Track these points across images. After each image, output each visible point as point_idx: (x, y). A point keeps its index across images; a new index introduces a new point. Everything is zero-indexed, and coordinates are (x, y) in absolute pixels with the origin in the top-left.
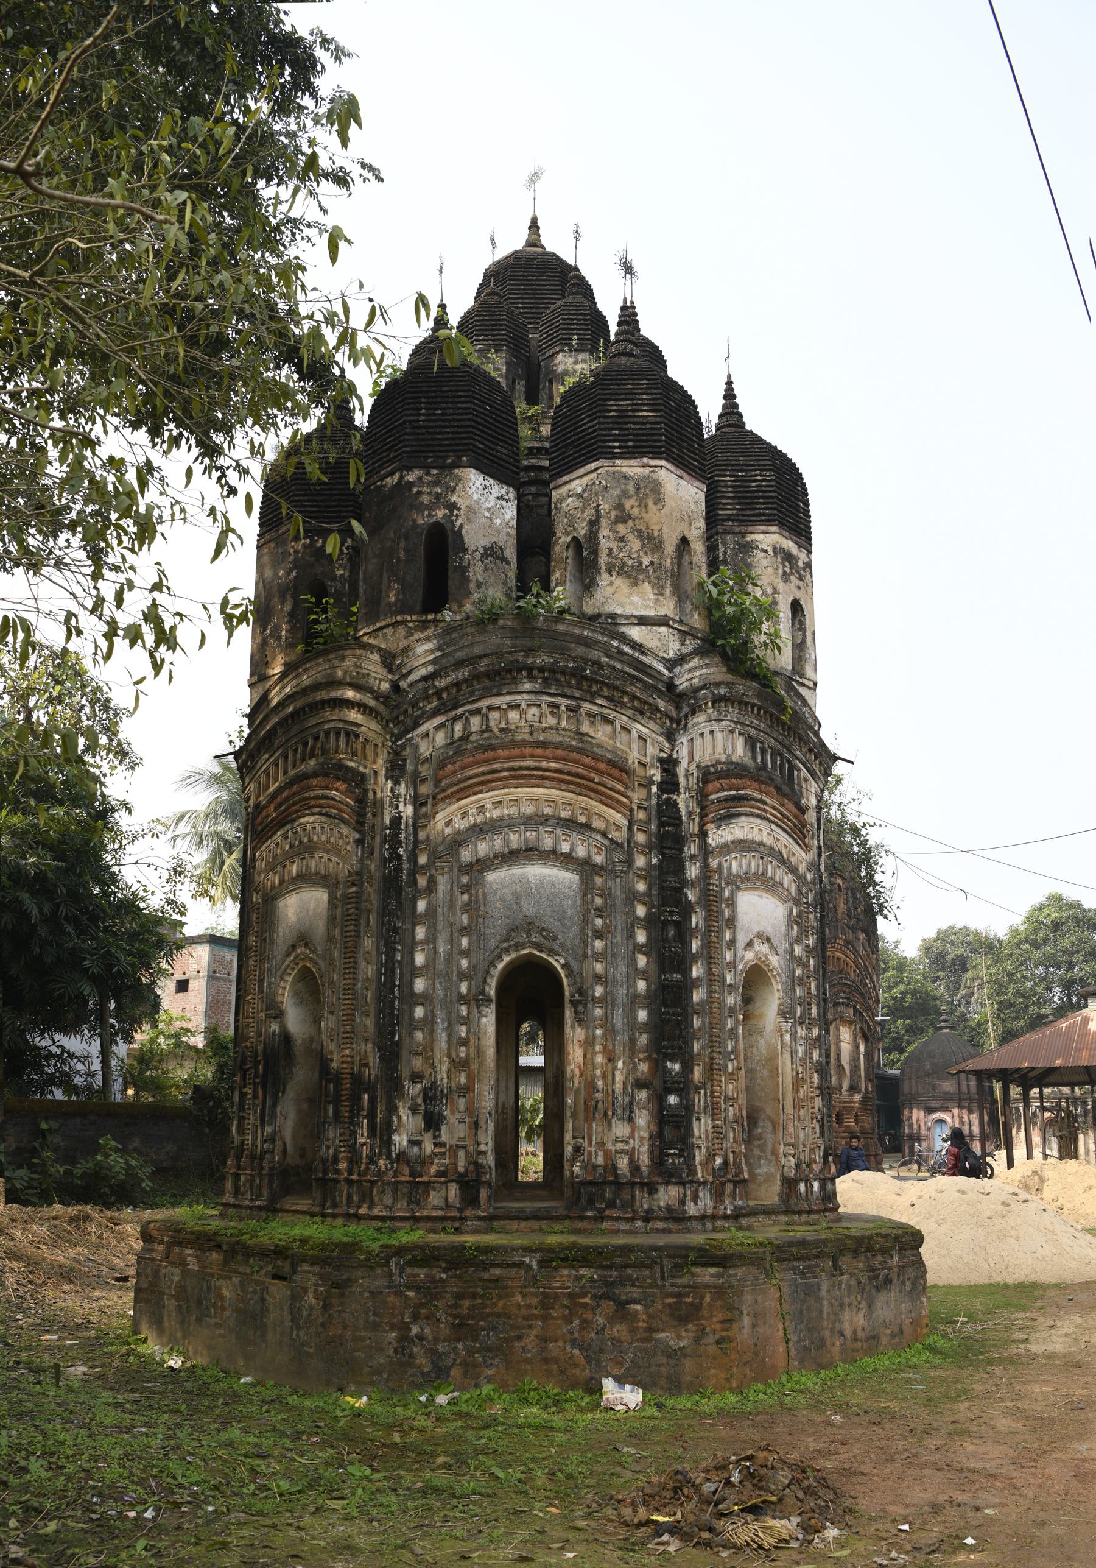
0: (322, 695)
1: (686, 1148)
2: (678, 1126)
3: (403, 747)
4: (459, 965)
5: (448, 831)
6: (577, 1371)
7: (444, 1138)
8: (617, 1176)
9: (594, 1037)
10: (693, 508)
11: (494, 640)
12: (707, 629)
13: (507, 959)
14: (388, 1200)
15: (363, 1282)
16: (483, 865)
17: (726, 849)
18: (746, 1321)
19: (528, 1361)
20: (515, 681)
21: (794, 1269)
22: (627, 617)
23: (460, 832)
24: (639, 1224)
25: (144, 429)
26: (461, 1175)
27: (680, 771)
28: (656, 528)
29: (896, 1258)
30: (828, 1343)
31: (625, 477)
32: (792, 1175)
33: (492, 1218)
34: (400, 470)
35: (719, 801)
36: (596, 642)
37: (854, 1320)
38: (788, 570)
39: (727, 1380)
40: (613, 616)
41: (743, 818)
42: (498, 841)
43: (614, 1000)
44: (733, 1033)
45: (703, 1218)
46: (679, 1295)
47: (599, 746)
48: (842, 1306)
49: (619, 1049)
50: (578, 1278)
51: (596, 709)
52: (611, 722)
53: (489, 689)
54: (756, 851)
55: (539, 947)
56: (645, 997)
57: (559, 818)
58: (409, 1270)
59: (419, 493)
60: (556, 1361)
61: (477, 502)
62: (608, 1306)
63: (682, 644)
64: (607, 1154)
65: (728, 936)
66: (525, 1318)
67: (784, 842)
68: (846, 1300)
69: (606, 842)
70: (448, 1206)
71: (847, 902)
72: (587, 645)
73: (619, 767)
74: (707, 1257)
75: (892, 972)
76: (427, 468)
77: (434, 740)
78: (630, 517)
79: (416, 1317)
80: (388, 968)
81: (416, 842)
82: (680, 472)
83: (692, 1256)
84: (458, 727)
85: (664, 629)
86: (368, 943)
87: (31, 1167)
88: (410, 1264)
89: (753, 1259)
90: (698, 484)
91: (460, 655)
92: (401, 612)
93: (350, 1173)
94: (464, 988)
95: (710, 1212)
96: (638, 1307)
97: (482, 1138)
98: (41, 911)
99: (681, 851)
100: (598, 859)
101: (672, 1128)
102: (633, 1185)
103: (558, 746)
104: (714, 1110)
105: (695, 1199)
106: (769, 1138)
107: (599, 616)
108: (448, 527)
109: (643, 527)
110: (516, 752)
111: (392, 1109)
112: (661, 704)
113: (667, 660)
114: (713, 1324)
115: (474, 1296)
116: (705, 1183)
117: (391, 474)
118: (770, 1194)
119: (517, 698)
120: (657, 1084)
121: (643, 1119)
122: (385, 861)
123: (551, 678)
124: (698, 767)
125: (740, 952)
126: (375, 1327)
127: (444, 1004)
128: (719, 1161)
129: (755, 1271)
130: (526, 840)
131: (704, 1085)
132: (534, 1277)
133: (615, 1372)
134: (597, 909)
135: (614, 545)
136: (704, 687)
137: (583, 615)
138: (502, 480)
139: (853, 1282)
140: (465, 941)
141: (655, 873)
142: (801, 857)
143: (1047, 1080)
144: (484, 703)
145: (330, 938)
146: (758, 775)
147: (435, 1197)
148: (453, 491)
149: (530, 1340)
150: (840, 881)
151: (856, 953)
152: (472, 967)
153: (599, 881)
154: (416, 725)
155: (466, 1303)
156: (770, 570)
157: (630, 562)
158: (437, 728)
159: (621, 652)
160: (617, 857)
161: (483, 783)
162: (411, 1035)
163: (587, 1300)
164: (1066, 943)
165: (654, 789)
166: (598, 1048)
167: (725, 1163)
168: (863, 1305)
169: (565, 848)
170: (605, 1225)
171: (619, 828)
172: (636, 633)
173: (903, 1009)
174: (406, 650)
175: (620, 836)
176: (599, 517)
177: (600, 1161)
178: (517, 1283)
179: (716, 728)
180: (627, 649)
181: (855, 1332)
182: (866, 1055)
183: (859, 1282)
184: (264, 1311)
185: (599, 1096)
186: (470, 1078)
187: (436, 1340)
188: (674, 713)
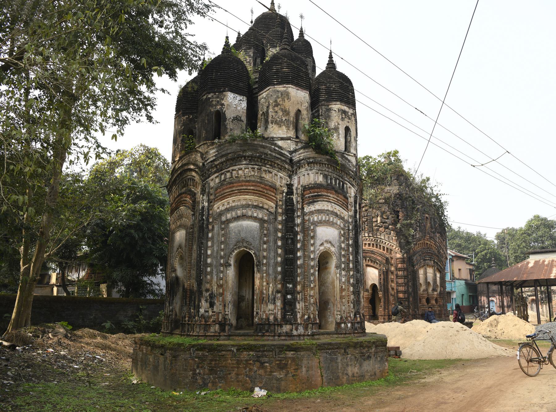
0: (186, 168)
1: (294, 313)
2: (291, 305)
3: (205, 184)
4: (220, 254)
5: (218, 211)
6: (247, 385)
7: (215, 310)
8: (269, 322)
9: (263, 276)
10: (303, 99)
11: (234, 148)
12: (308, 140)
13: (236, 252)
14: (198, 330)
15: (183, 356)
16: (228, 221)
17: (312, 213)
18: (304, 369)
19: (232, 381)
20: (240, 161)
21: (326, 353)
22: (277, 138)
23: (222, 211)
24: (276, 337)
25: (177, 70)
26: (220, 322)
27: (294, 188)
28: (287, 108)
29: (373, 349)
30: (341, 377)
31: (278, 91)
32: (339, 321)
33: (230, 336)
34: (206, 94)
35: (309, 197)
36: (267, 147)
37: (352, 370)
38: (344, 117)
39: (295, 388)
40: (273, 138)
41: (320, 202)
42: (234, 213)
43: (269, 264)
44: (313, 274)
45: (299, 336)
46: (280, 361)
47: (267, 181)
48: (347, 365)
49: (271, 281)
50: (249, 355)
51: (267, 169)
52: (271, 173)
53: (232, 164)
54: (325, 213)
55: (246, 247)
56: (280, 263)
57: (253, 205)
58: (197, 352)
59: (212, 101)
60: (241, 381)
61: (231, 103)
62: (258, 364)
63: (296, 145)
64: (266, 314)
65: (312, 242)
66: (232, 368)
67: (338, 209)
68: (350, 363)
69: (268, 212)
70: (216, 332)
71: (431, 223)
72: (264, 148)
73: (273, 188)
74: (290, 348)
75: (482, 246)
76: (215, 93)
77: (215, 181)
78: (279, 104)
79: (198, 367)
80: (199, 255)
81: (209, 214)
82: (297, 88)
83: (285, 348)
84: (223, 177)
85: (289, 141)
86: (195, 247)
87: (135, 321)
88: (197, 350)
89: (308, 349)
90: (305, 91)
91: (223, 153)
92: (205, 140)
93: (189, 321)
94: (222, 261)
95: (302, 333)
96: (267, 364)
97: (227, 310)
98: (138, 236)
99: (294, 214)
100: (266, 218)
101: (289, 306)
102: (275, 325)
103: (253, 181)
104: (305, 299)
105: (297, 329)
106: (332, 308)
107: (268, 138)
108: (221, 111)
109: (283, 108)
110: (240, 184)
111: (200, 301)
112: (287, 166)
113: (290, 151)
114: (291, 370)
115: (216, 360)
116: (301, 324)
117: (205, 95)
118: (332, 328)
119: (241, 166)
120: (283, 291)
121: (279, 303)
122: (200, 221)
123: (251, 159)
124: (302, 186)
125: (318, 247)
126: (186, 370)
127: (216, 266)
128: (306, 317)
129: (309, 353)
130: (243, 213)
131: (301, 292)
132: (235, 354)
133: (260, 385)
134: (265, 235)
135: (273, 114)
136: (303, 159)
137: (264, 138)
138: (240, 94)
139: (353, 357)
140: (223, 246)
141: (284, 222)
142: (345, 214)
143: (524, 285)
144: (231, 169)
145: (186, 246)
146: (329, 187)
147: (212, 329)
148: (223, 100)
149: (233, 375)
150: (427, 215)
151: (435, 241)
152: (225, 254)
153: (266, 225)
154: (209, 177)
155: (213, 363)
156: (337, 117)
157: (279, 120)
158: (216, 177)
159: (275, 150)
160: (272, 217)
161: (229, 195)
162: (206, 277)
163: (251, 362)
164: (540, 233)
165: (284, 194)
166: (264, 280)
167: (309, 317)
168: (357, 365)
169: (255, 215)
170: (265, 338)
171: (272, 208)
172: (280, 143)
173: (487, 259)
174: (207, 152)
175: (273, 210)
176: (269, 105)
177: (264, 317)
178: (230, 356)
179: (310, 172)
180: (277, 148)
181: (353, 374)
182: (440, 278)
183: (355, 357)
184: (159, 365)
185: (264, 296)
186: (223, 290)
187: (204, 374)
188: (291, 169)
